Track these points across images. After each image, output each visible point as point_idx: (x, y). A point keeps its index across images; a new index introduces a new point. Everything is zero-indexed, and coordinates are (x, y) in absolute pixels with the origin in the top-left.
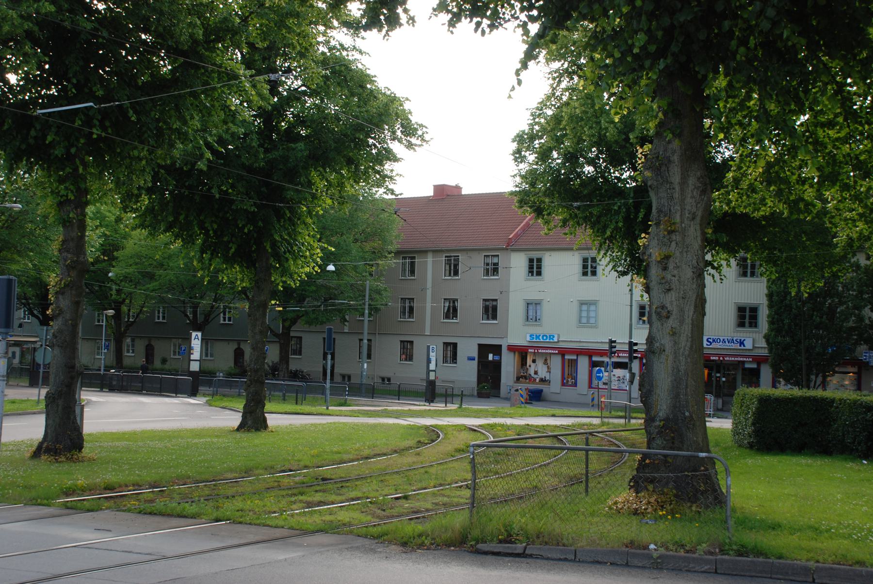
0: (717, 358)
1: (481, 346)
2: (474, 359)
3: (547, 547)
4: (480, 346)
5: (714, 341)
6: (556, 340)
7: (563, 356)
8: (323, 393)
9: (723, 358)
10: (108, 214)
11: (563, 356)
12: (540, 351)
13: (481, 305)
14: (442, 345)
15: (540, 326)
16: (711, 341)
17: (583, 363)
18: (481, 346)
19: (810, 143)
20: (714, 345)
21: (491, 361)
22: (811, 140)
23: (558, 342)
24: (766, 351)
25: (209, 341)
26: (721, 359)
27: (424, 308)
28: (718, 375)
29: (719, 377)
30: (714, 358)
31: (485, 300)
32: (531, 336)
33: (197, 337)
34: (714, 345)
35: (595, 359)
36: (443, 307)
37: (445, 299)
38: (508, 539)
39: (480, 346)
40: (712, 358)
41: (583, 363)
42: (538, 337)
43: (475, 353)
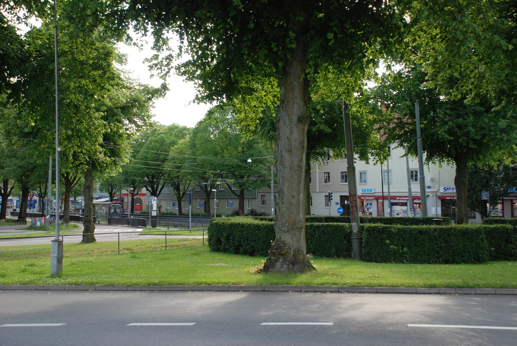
0: (450, 198)
1: (341, 197)
2: (338, 204)
3: (503, 289)
4: (341, 196)
5: (448, 189)
6: (373, 192)
7: (377, 200)
8: (188, 227)
9: (453, 198)
10: (166, 139)
11: (377, 200)
12: (402, 198)
13: (340, 175)
14: (324, 196)
15: (366, 184)
16: (446, 189)
17: (386, 203)
18: (341, 197)
19: (196, 39)
20: (448, 191)
21: (346, 205)
22: (194, 38)
23: (375, 193)
24: (420, 194)
25: (250, 200)
26: (452, 198)
27: (316, 177)
28: (454, 207)
29: (454, 209)
30: (448, 198)
31: (342, 172)
32: (362, 190)
33: (154, 200)
34: (448, 191)
35: (392, 201)
36: (324, 177)
37: (324, 173)
38: (479, 285)
39: (341, 196)
40: (447, 198)
41: (386, 203)
42: (365, 191)
43: (338, 201)
